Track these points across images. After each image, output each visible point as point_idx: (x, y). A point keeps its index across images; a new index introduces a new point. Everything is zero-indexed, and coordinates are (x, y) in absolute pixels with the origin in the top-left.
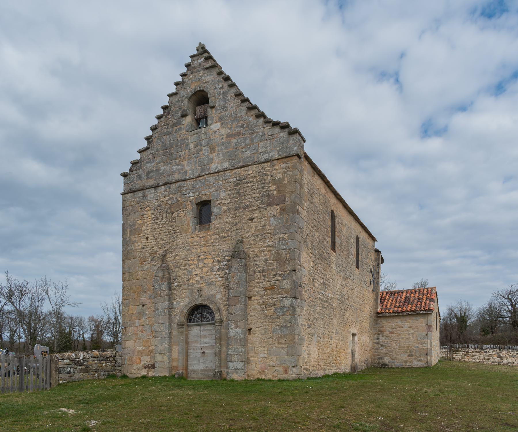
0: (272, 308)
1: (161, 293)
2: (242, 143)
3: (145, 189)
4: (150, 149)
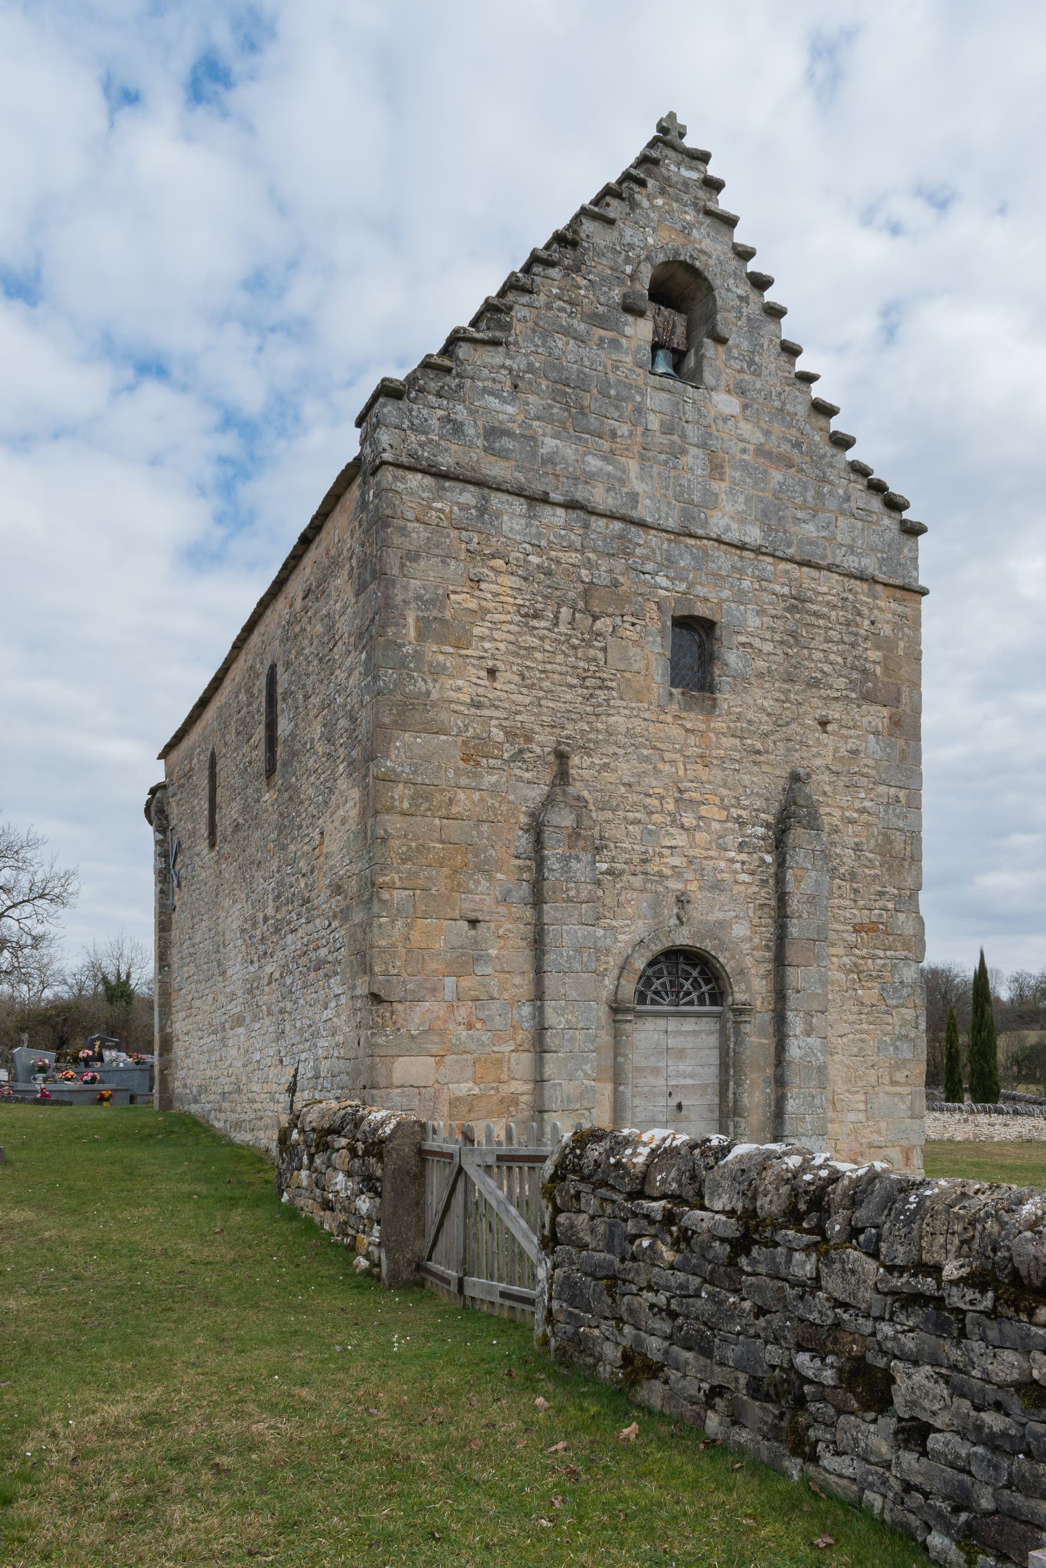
1: (568, 889)
4: (502, 349)
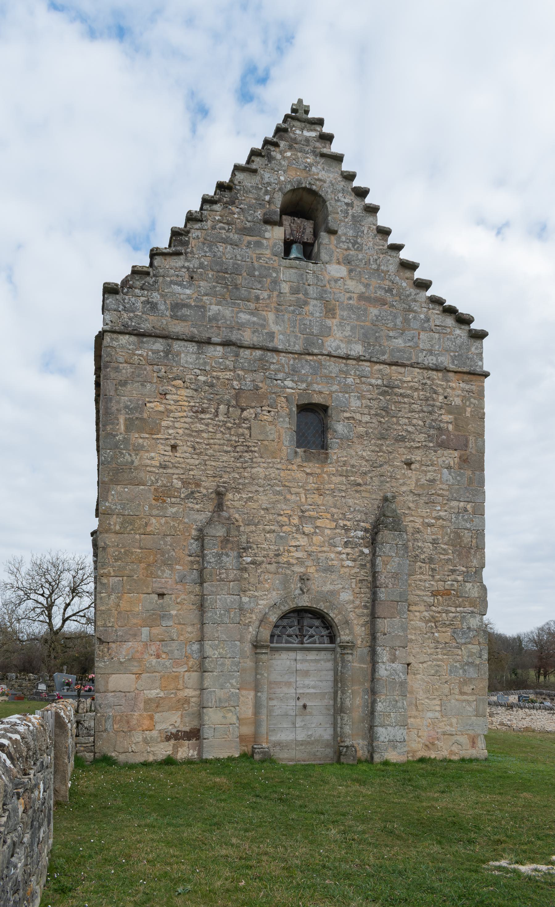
0: (448, 629)
1: (220, 574)
2: (388, 320)
3: (172, 339)
4: (182, 257)
